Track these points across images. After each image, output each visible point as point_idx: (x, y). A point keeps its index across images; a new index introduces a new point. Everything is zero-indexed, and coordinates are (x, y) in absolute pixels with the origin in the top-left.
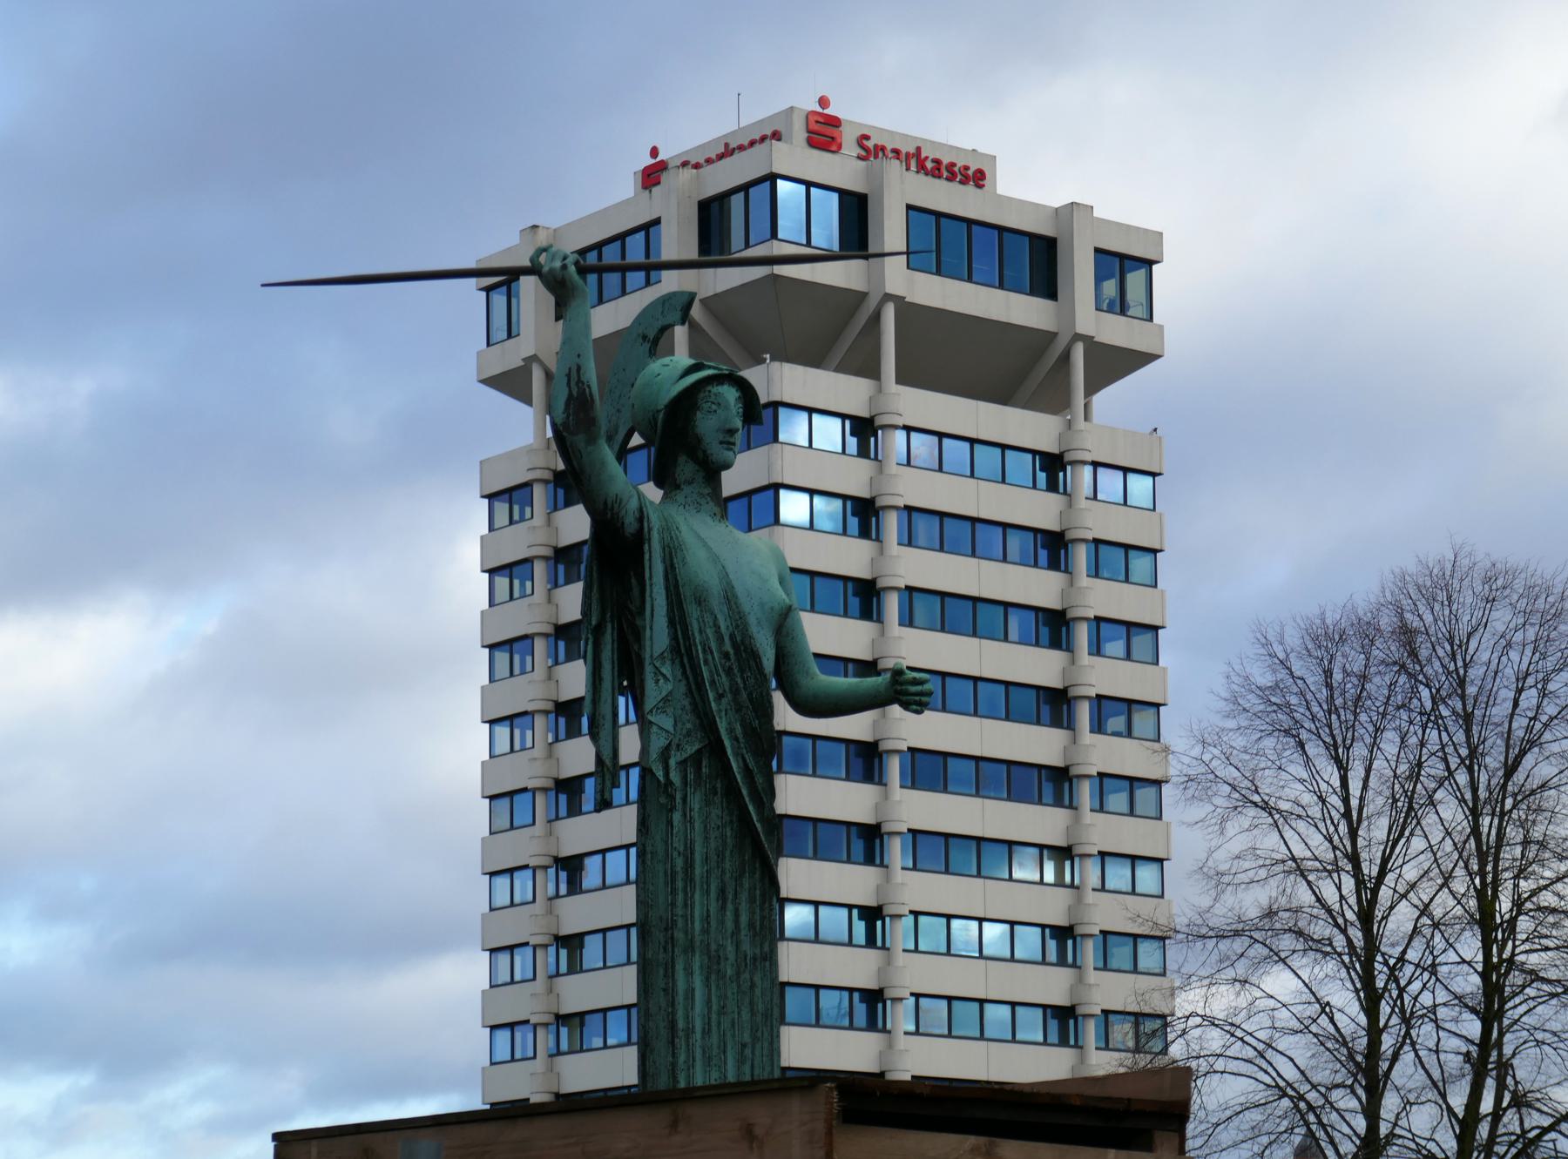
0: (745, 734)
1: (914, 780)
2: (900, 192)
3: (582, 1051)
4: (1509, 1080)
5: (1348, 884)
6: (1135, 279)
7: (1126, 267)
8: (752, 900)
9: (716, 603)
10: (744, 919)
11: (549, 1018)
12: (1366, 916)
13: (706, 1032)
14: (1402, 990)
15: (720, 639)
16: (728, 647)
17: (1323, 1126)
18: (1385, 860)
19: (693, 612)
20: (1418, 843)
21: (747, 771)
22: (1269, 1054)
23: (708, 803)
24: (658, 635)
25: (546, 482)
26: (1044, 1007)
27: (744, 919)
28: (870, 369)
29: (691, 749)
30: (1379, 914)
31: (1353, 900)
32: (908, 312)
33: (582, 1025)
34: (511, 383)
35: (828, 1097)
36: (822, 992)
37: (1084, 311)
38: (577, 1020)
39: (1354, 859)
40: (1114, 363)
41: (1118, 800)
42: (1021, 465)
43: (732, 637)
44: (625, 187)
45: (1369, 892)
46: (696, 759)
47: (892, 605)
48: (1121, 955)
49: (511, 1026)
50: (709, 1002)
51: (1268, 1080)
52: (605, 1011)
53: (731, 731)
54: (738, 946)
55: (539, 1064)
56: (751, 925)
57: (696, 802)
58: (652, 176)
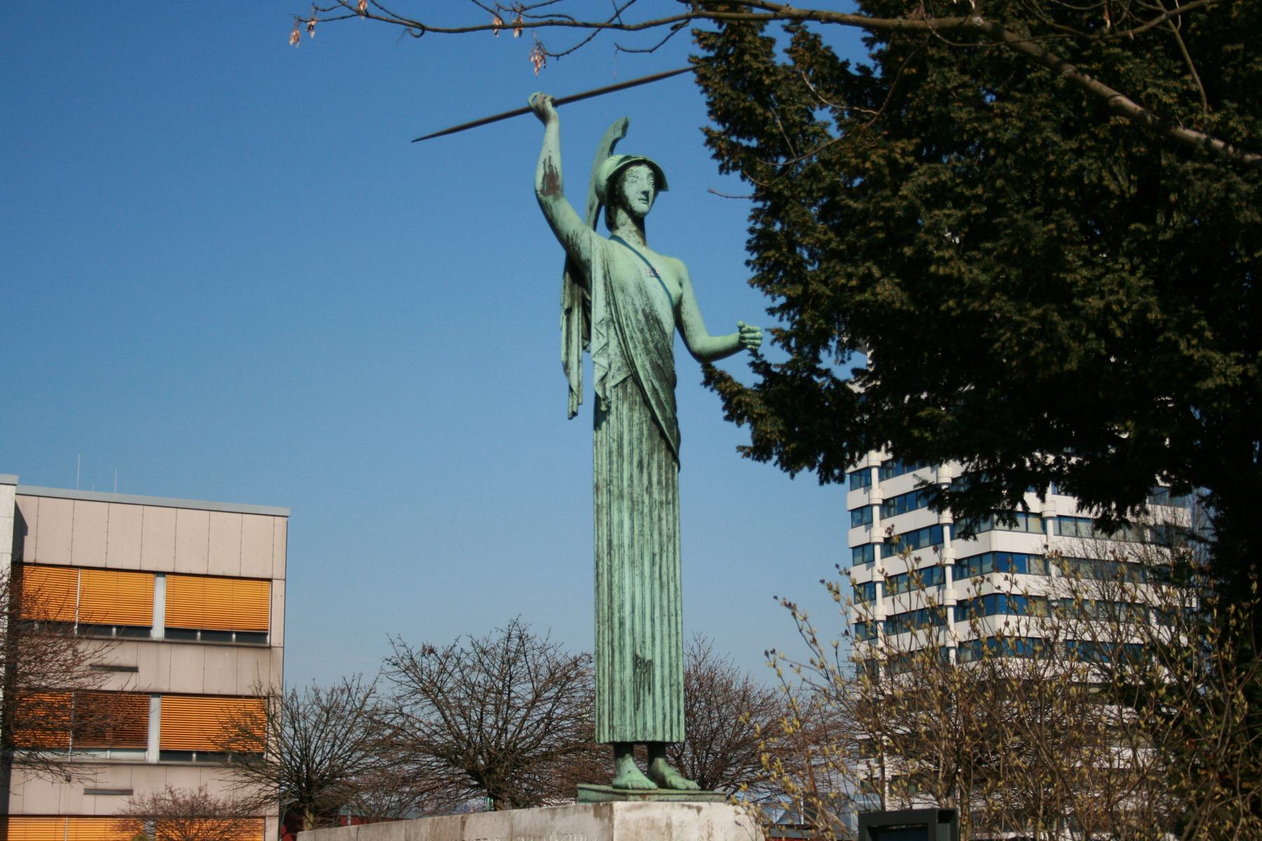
0: (653, 368)
8: (660, 467)
9: (632, 289)
10: (655, 479)
13: (632, 546)
15: (636, 312)
16: (641, 316)
19: (620, 297)
21: (655, 390)
23: (631, 410)
27: (655, 479)
29: (620, 378)
43: (643, 311)
50: (632, 528)
53: (643, 366)
54: (650, 494)
56: (659, 482)
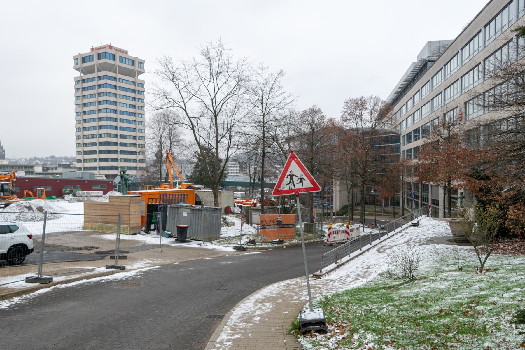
1: (120, 130)
2: (118, 55)
6: (142, 65)
7: (141, 63)
28: (115, 72)
32: (119, 66)
34: (77, 69)
37: (137, 68)
40: (140, 73)
41: (140, 101)
42: (131, 99)
44: (89, 51)
47: (118, 88)
55: (82, 140)
58: (92, 49)
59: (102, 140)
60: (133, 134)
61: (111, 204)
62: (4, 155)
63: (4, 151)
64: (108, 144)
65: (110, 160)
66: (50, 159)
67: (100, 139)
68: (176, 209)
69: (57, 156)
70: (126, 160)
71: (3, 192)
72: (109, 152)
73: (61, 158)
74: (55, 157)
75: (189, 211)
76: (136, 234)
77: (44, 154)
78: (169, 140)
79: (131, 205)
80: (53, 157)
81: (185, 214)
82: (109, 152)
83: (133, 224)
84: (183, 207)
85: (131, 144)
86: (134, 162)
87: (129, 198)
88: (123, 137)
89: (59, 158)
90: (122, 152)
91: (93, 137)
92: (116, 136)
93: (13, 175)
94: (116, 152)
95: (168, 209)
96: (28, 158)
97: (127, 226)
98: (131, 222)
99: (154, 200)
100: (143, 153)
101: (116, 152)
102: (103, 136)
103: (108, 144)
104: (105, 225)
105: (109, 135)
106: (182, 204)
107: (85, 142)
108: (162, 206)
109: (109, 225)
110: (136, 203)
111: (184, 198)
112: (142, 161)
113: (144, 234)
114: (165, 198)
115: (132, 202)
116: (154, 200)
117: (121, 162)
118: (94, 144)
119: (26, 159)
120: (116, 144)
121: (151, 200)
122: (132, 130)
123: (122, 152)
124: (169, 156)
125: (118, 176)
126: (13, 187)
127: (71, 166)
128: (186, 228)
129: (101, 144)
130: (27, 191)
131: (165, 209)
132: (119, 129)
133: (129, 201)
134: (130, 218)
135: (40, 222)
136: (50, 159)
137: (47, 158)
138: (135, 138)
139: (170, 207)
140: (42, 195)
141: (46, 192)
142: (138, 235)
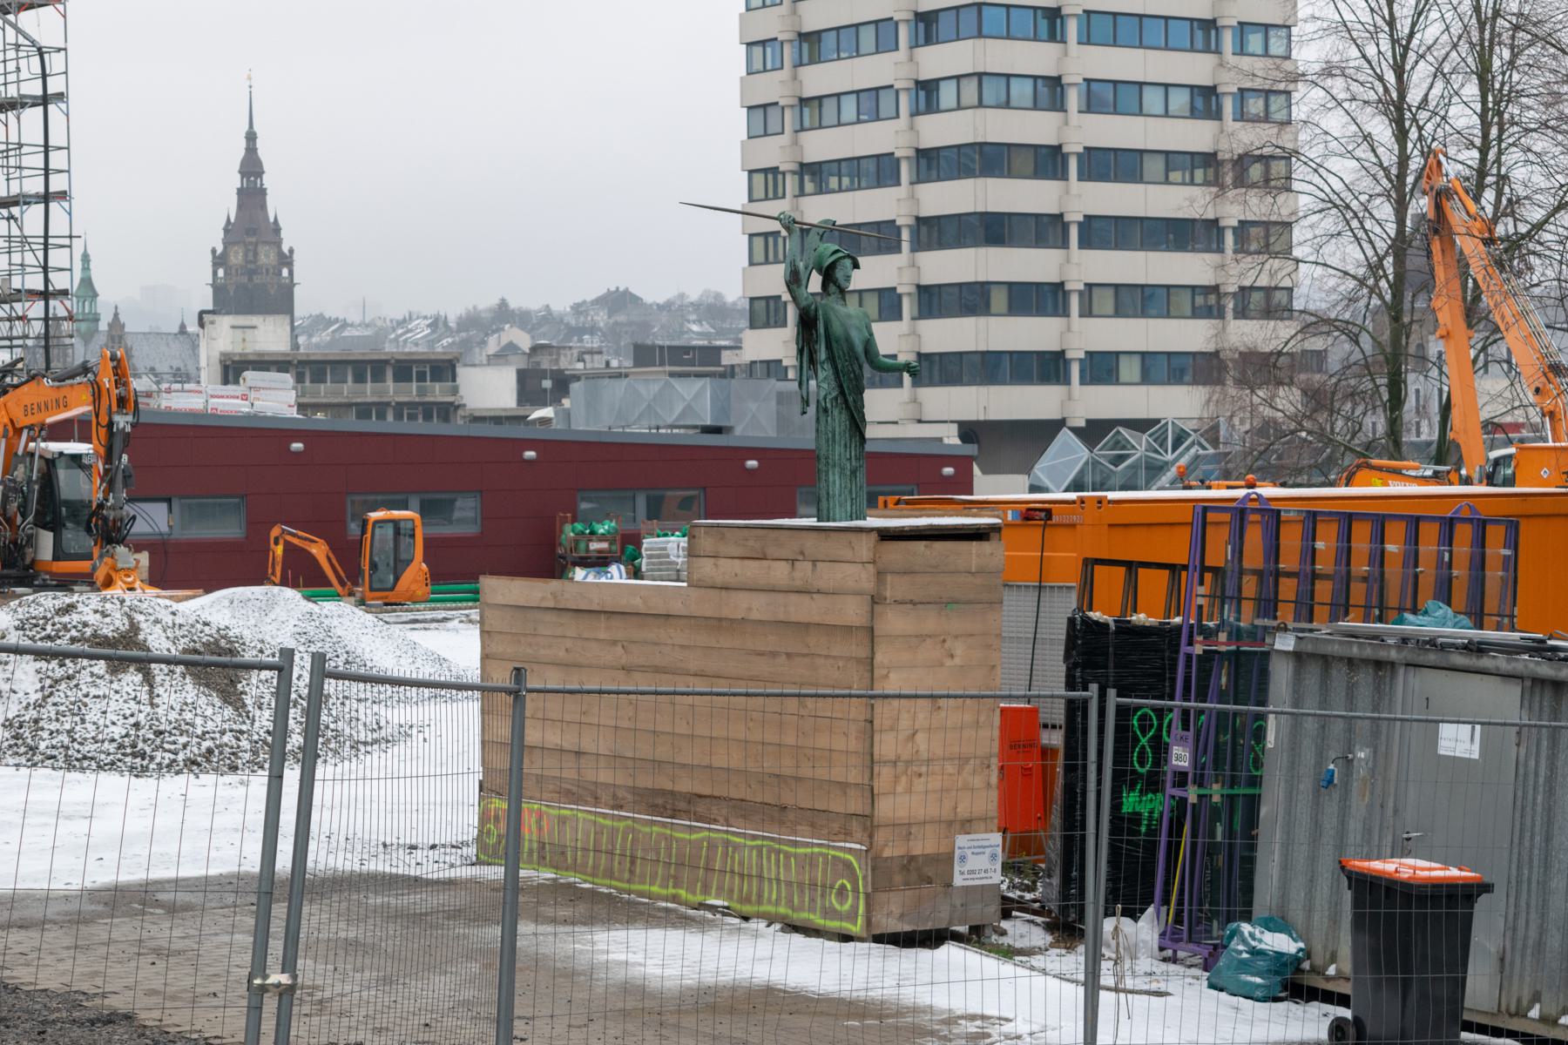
3: (821, 127)
4: (1507, 189)
5: (1385, 45)
11: (795, 101)
12: (1399, 70)
14: (1420, 128)
17: (1366, 231)
18: (1413, 25)
20: (1434, 15)
22: (1321, 170)
24: (822, 355)
25: (794, 173)
26: (1192, 87)
29: (834, 394)
30: (1408, 67)
31: (1389, 54)
33: (820, 106)
35: (874, 535)
36: (1013, 80)
38: (816, 103)
39: (1391, 23)
45: (1402, 47)
46: (836, 398)
48: (1255, 42)
49: (763, 43)
51: (1323, 195)
52: (838, 95)
55: (784, 140)
57: (836, 412)
59: (943, 130)
60: (1194, 68)
61: (708, 605)
62: (287, 291)
63: (287, 260)
64: (989, 159)
65: (999, 299)
66: (601, 318)
67: (924, 121)
68: (1364, 678)
69: (653, 292)
70: (1139, 300)
71: (55, 526)
72: (994, 229)
73: (675, 309)
74: (636, 300)
75: (1506, 701)
76: (932, 939)
77: (557, 284)
78: (1472, 90)
79: (893, 622)
80: (619, 300)
81: (1458, 741)
82: (994, 229)
83: (906, 829)
84: (1432, 655)
85: (1171, 158)
86: (1196, 313)
87: (865, 547)
88: (1109, 96)
89: (666, 307)
90: (1103, 232)
91: (872, 103)
92: (1051, 92)
93: (107, 382)
94: (1045, 230)
95: (1281, 676)
96: (453, 313)
97: (850, 849)
98: (886, 808)
99: (1153, 584)
100: (1268, 237)
101: (1045, 230)
102: (947, 94)
103: (989, 159)
104: (653, 827)
105: (990, 87)
106: (1440, 623)
107: (811, 157)
108: (1223, 644)
109: (687, 833)
110: (943, 604)
111: (1479, 564)
112: (1269, 303)
113: (1039, 937)
114: (1254, 556)
115: (895, 588)
116: (1153, 584)
117: (1087, 312)
118: (881, 170)
119: (437, 323)
120: (1048, 161)
121: (1110, 581)
122: (1180, 33)
123: (1103, 232)
124: (1457, 217)
125: (1065, 436)
126: (109, 480)
127: (727, 358)
128: (1461, 897)
129: (933, 163)
130: (297, 537)
131: (1250, 672)
132: (1072, 28)
133: (863, 578)
134: (871, 762)
135: (204, 786)
136: (601, 318)
137: (578, 309)
138: (1205, 101)
139: (1298, 656)
140: (400, 565)
141: (433, 548)
142: (950, 952)
